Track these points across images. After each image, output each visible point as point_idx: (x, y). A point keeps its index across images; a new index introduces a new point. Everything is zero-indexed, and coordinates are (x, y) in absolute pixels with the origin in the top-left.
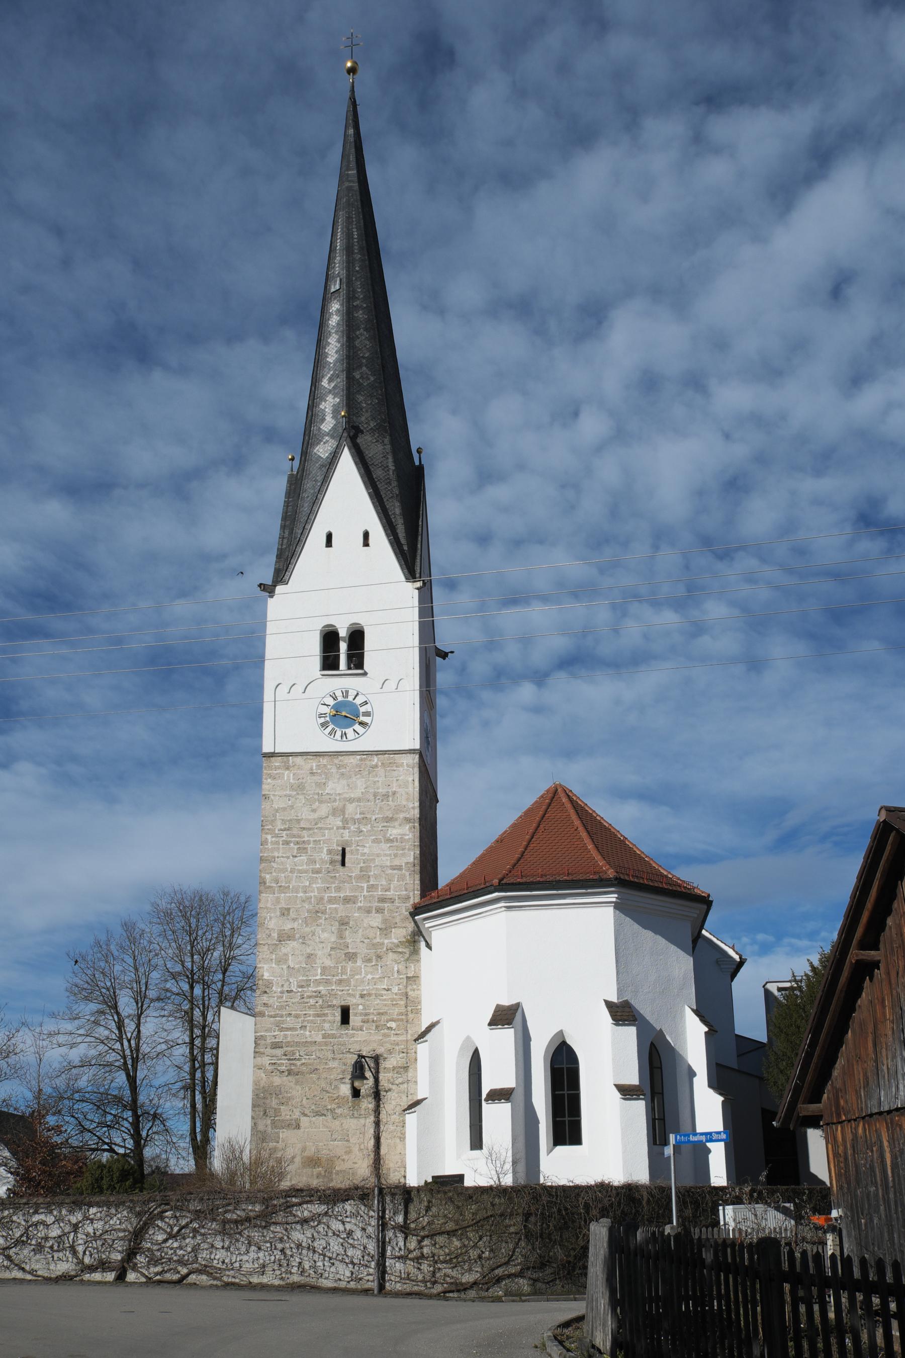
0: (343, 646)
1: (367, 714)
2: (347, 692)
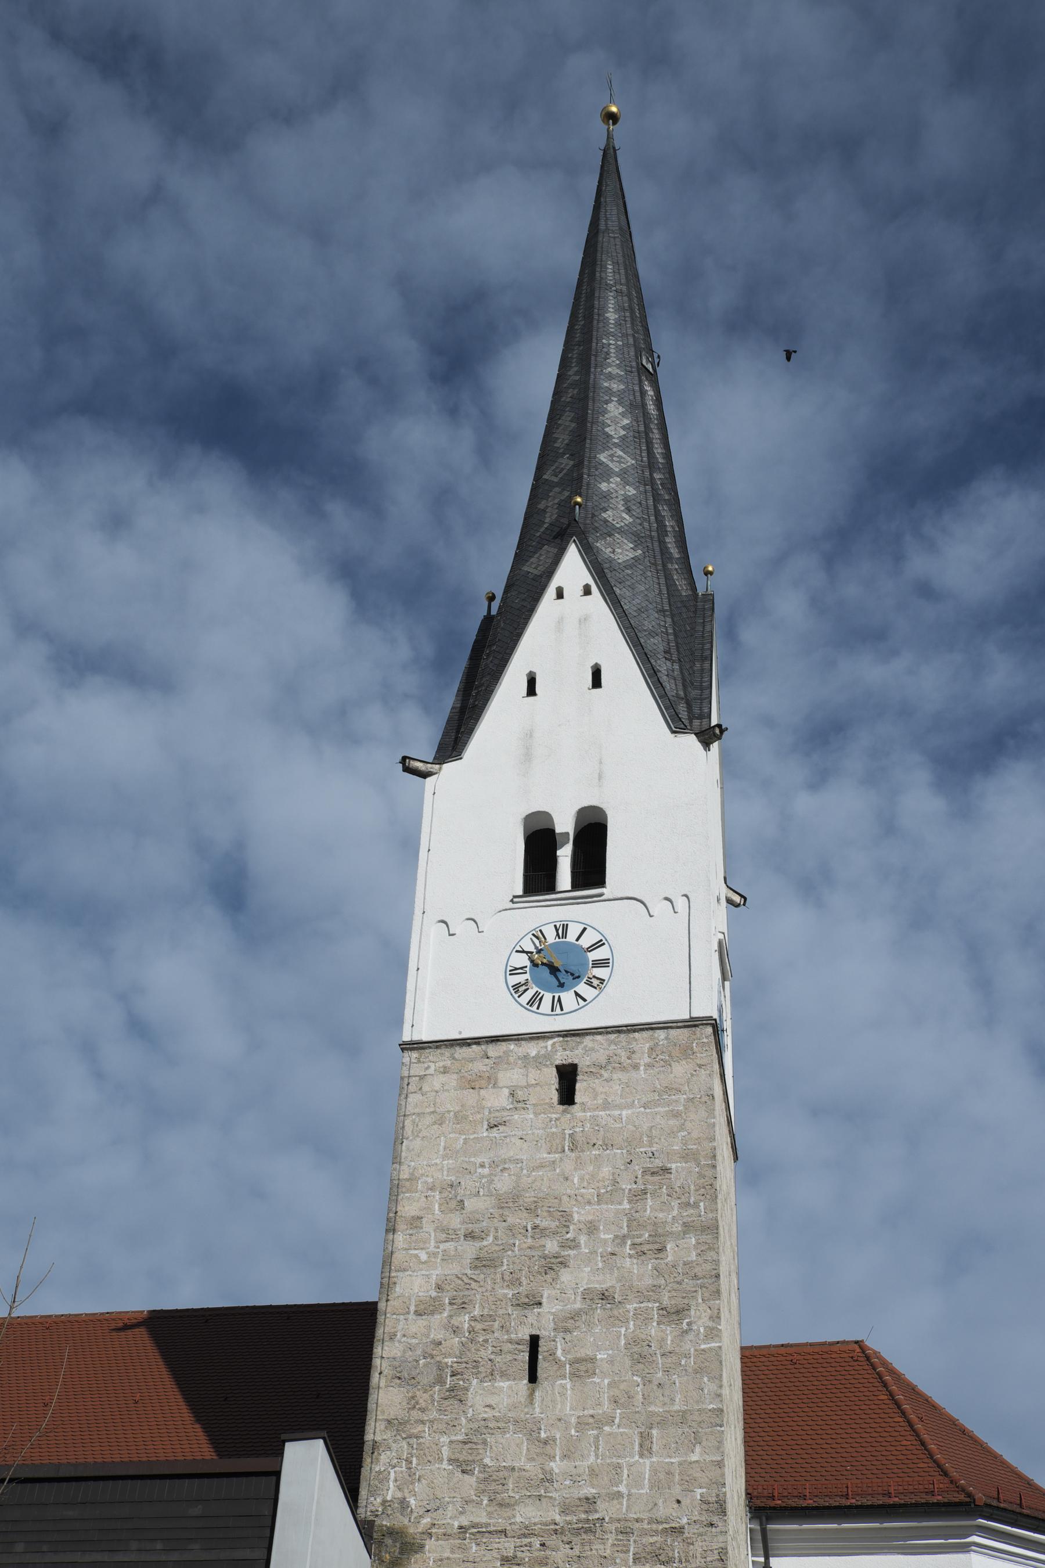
0: (565, 856)
1: (602, 963)
2: (565, 928)
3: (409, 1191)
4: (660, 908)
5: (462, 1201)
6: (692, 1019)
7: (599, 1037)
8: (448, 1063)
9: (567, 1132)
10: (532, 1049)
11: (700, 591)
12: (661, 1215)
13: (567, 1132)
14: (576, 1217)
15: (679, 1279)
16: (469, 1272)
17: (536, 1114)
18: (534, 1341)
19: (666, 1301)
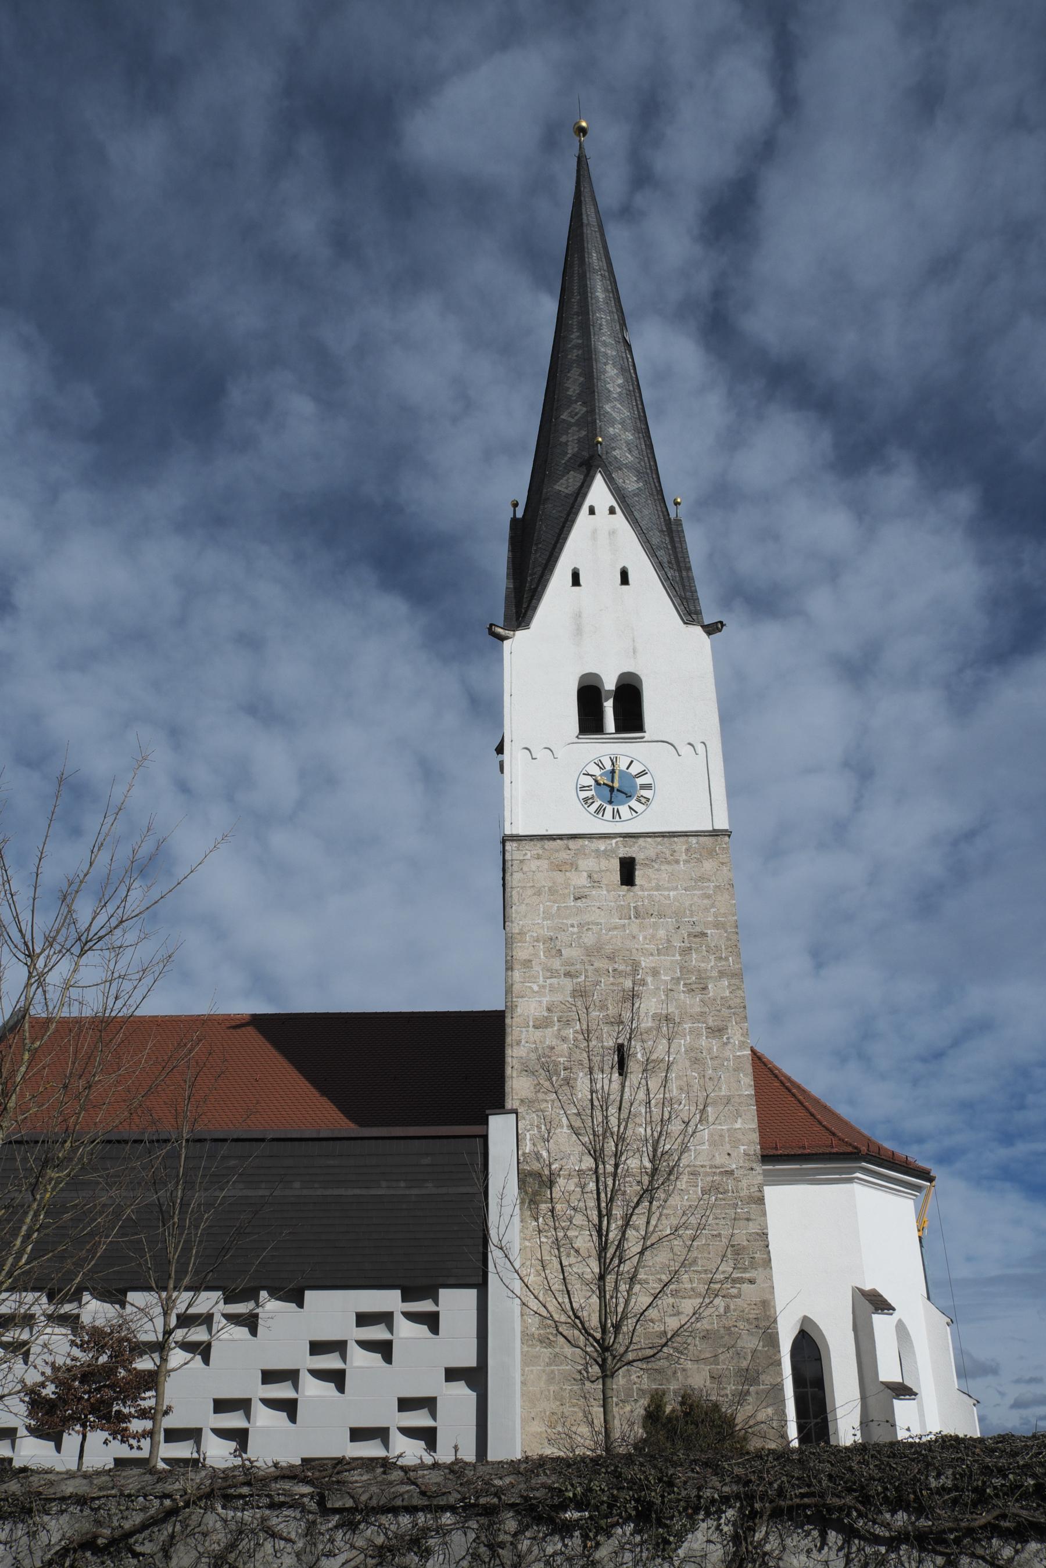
1: (646, 787)
3: (520, 941)
4: (685, 750)
5: (560, 950)
6: (714, 830)
7: (649, 840)
8: (540, 852)
9: (632, 905)
10: (602, 845)
11: (672, 516)
12: (703, 965)
13: (632, 905)
14: (643, 964)
15: (718, 1008)
16: (570, 1000)
17: (608, 891)
19: (711, 1023)
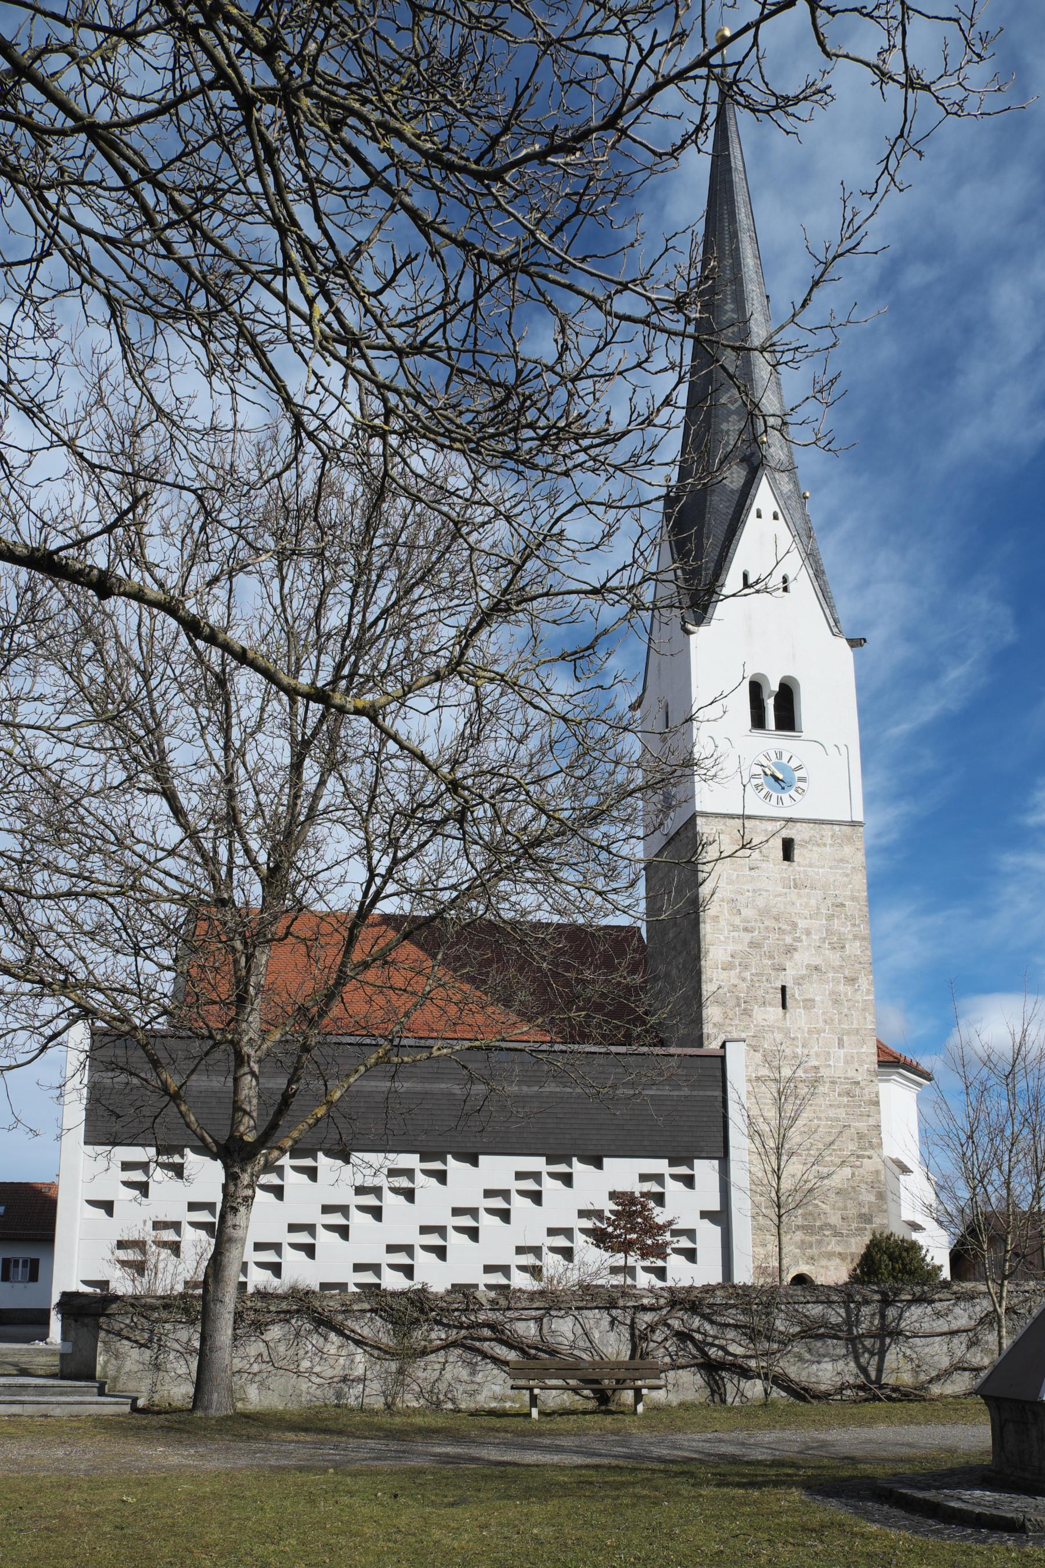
18: (783, 989)
